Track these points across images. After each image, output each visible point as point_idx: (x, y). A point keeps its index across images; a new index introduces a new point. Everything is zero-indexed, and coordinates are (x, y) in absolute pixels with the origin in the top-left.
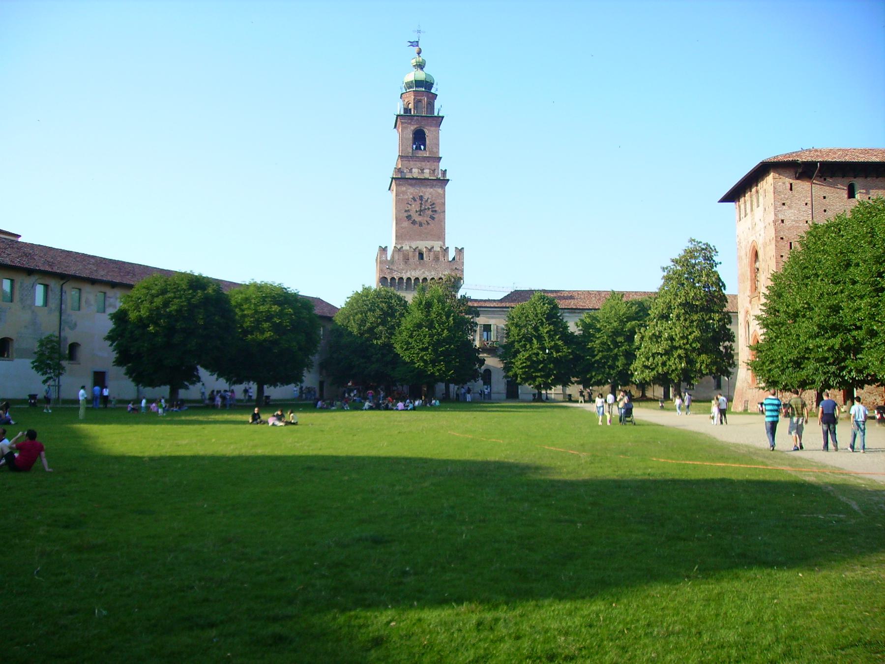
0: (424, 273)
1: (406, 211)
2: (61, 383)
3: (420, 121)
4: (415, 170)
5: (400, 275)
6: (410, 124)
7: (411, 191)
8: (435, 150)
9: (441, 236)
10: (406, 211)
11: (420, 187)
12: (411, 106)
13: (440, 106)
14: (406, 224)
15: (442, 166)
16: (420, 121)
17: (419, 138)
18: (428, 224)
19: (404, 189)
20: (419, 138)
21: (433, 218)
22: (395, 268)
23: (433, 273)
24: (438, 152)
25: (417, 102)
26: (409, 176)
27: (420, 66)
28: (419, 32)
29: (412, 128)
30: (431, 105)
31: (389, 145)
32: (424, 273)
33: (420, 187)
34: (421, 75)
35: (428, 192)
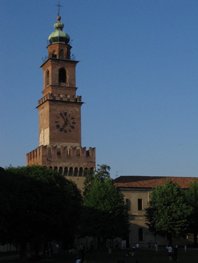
0: (71, 164)
1: (56, 122)
2: (27, 162)
3: (62, 61)
4: (61, 96)
5: (61, 165)
6: (57, 64)
7: (60, 109)
8: (73, 83)
9: (78, 139)
10: (56, 122)
11: (64, 108)
12: (56, 53)
13: (75, 54)
14: (56, 131)
15: (78, 93)
16: (62, 61)
17: (62, 76)
18: (70, 131)
19: (55, 107)
20: (62, 76)
21: (73, 128)
22: (52, 160)
23: (76, 164)
24: (75, 84)
25: (61, 51)
26: (58, 99)
27: (60, 28)
28: (59, 6)
29: (59, 67)
30: (68, 53)
31: (39, 82)
32: (71, 164)
33: (64, 108)
34: (63, 34)
35: (70, 110)
